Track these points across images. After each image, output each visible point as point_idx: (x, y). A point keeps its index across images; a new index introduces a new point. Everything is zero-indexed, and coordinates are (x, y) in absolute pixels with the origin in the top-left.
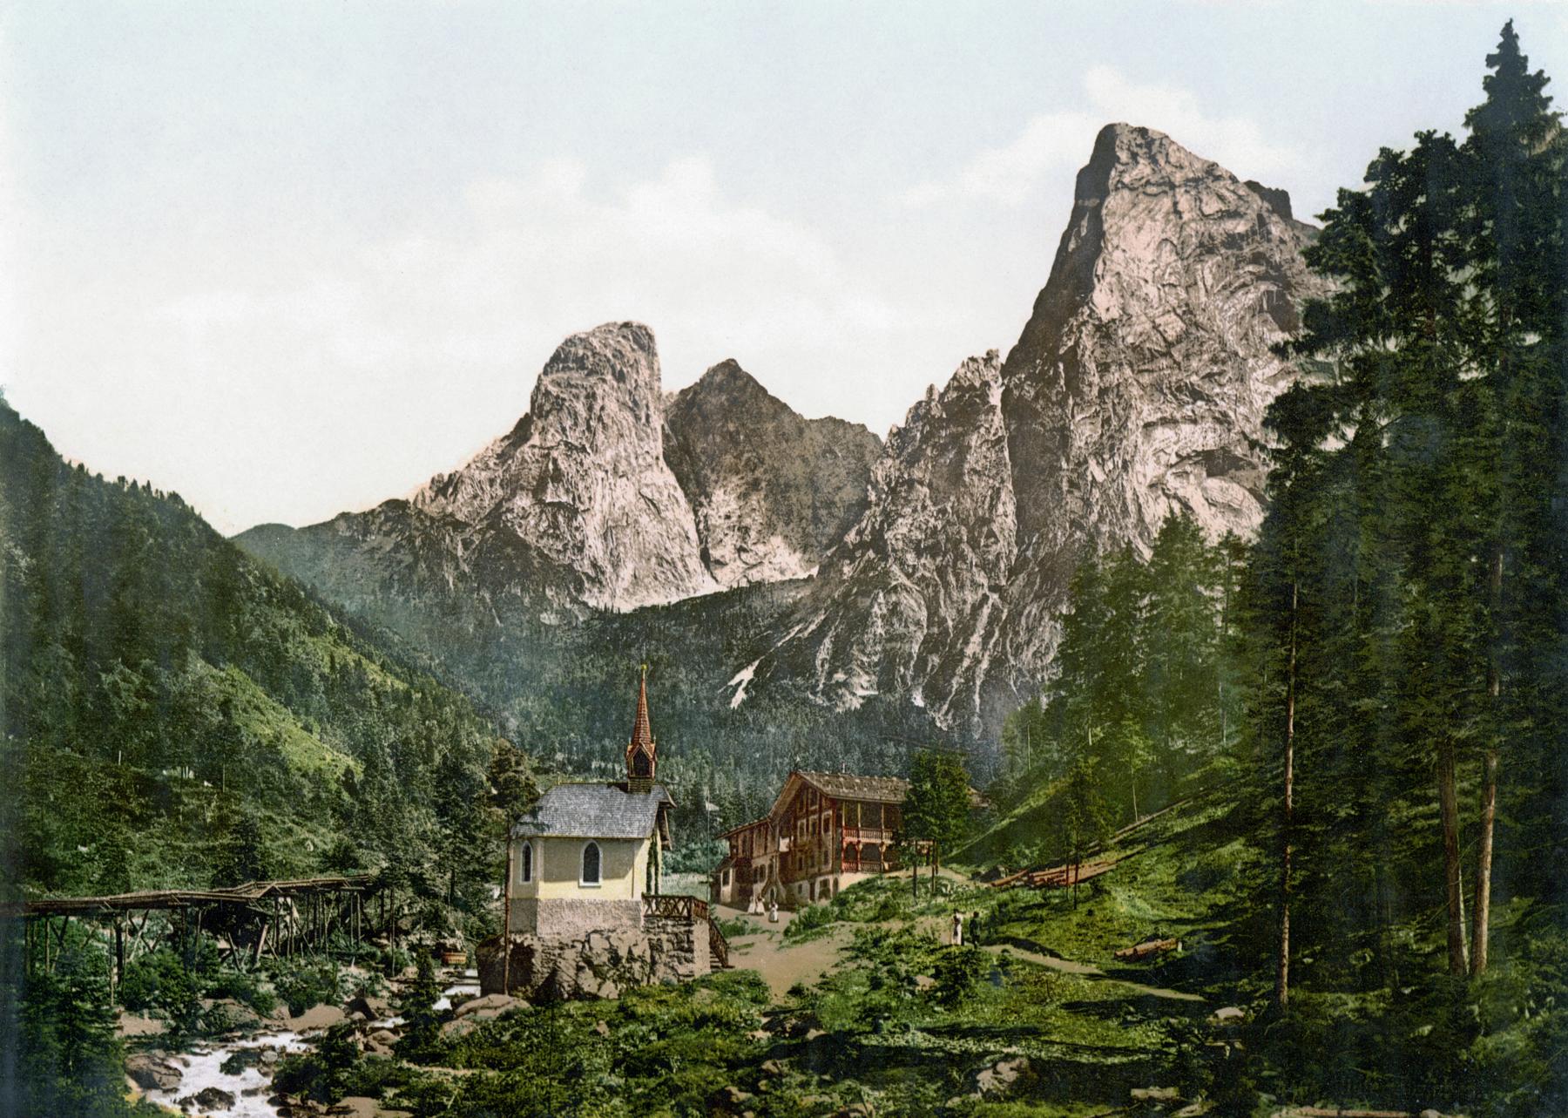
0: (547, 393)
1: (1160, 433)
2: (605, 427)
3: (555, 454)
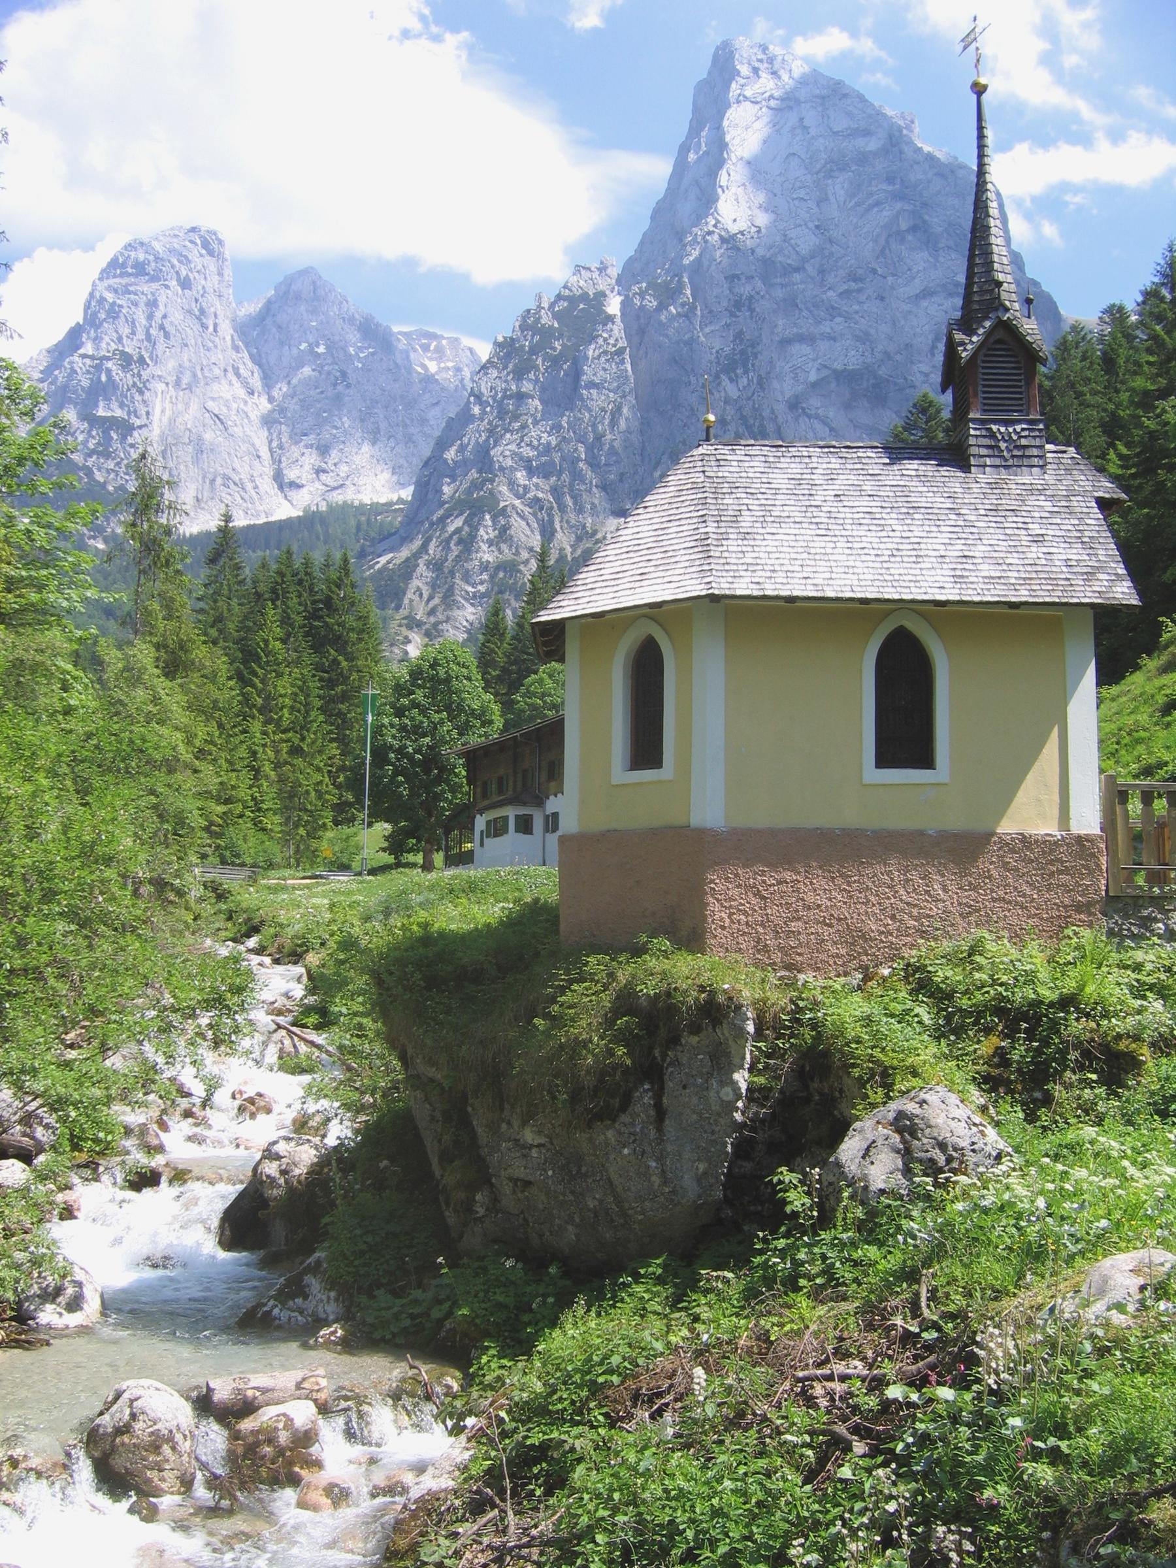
0: (102, 300)
1: (800, 351)
2: (167, 336)
3: (110, 364)
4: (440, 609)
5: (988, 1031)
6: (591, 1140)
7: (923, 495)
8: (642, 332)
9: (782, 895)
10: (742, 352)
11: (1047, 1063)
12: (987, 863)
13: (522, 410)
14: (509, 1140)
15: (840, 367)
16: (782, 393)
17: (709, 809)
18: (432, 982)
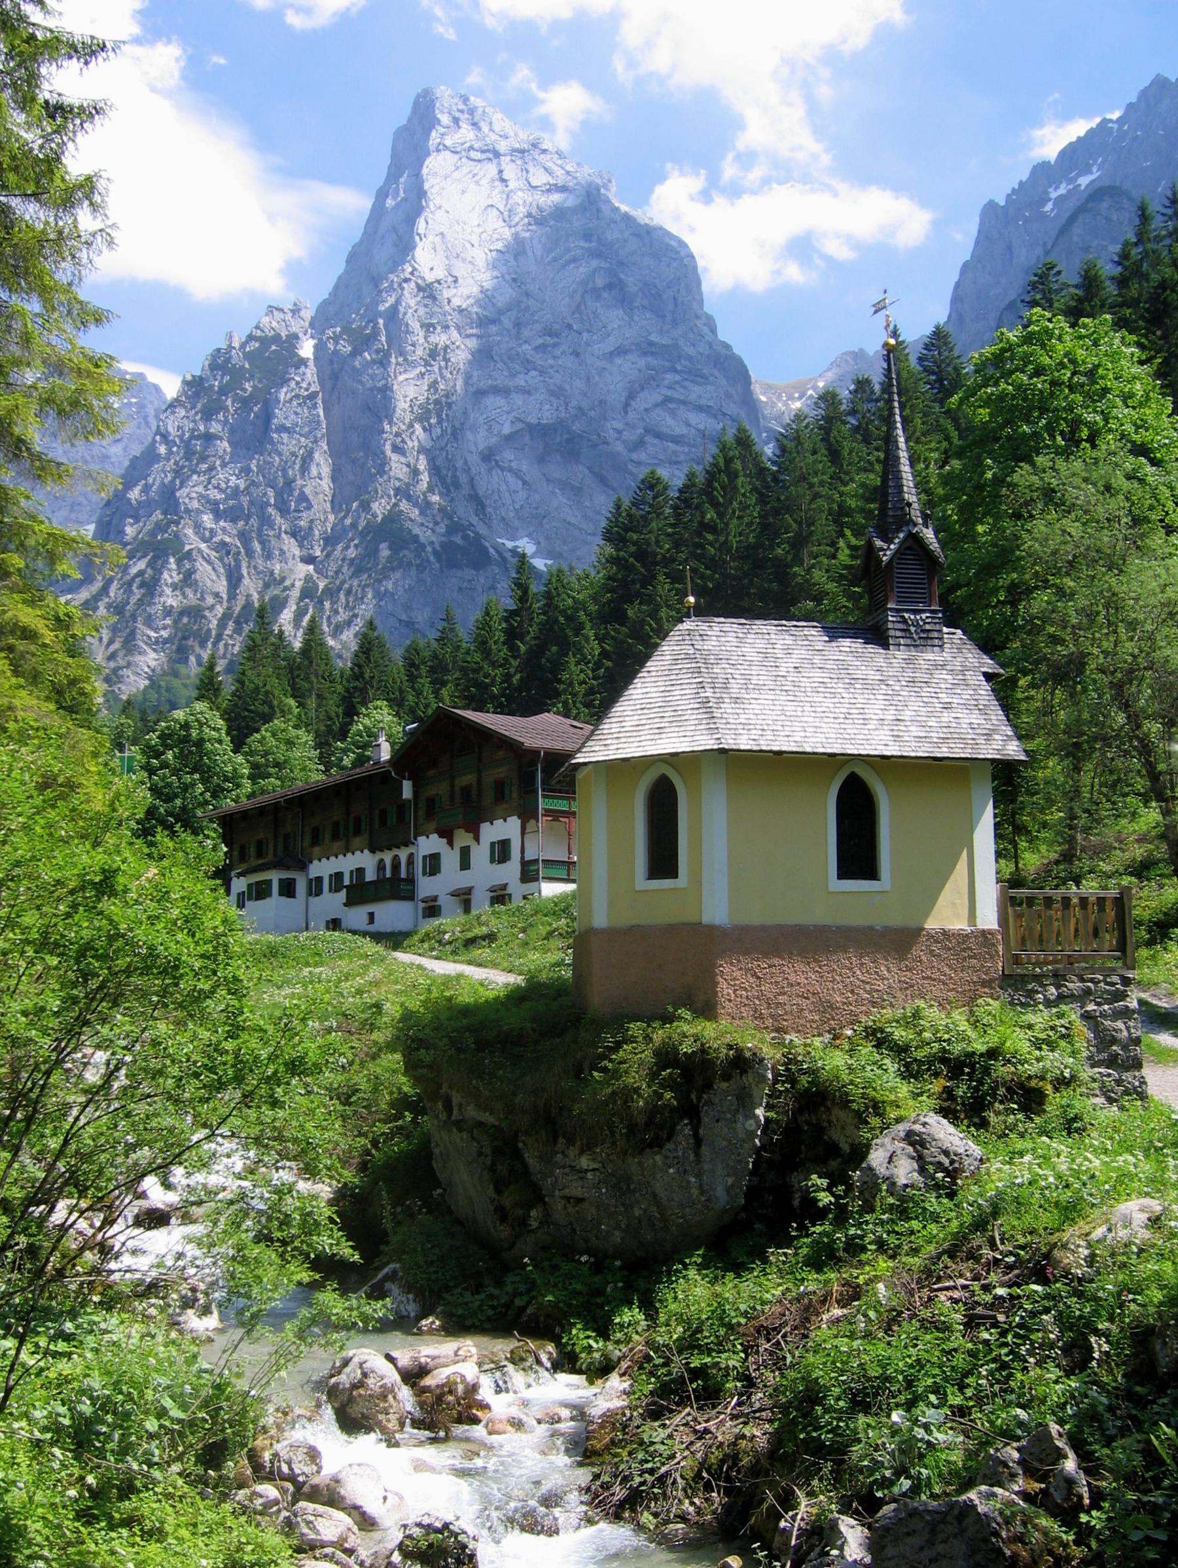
4: (121, 653)
5: (936, 1075)
6: (640, 1164)
7: (862, 670)
8: (335, 377)
9: (772, 975)
10: (437, 402)
11: (983, 1098)
12: (917, 951)
13: (211, 451)
14: (564, 1167)
15: (534, 421)
16: (476, 444)
17: (716, 910)
18: (482, 1045)
